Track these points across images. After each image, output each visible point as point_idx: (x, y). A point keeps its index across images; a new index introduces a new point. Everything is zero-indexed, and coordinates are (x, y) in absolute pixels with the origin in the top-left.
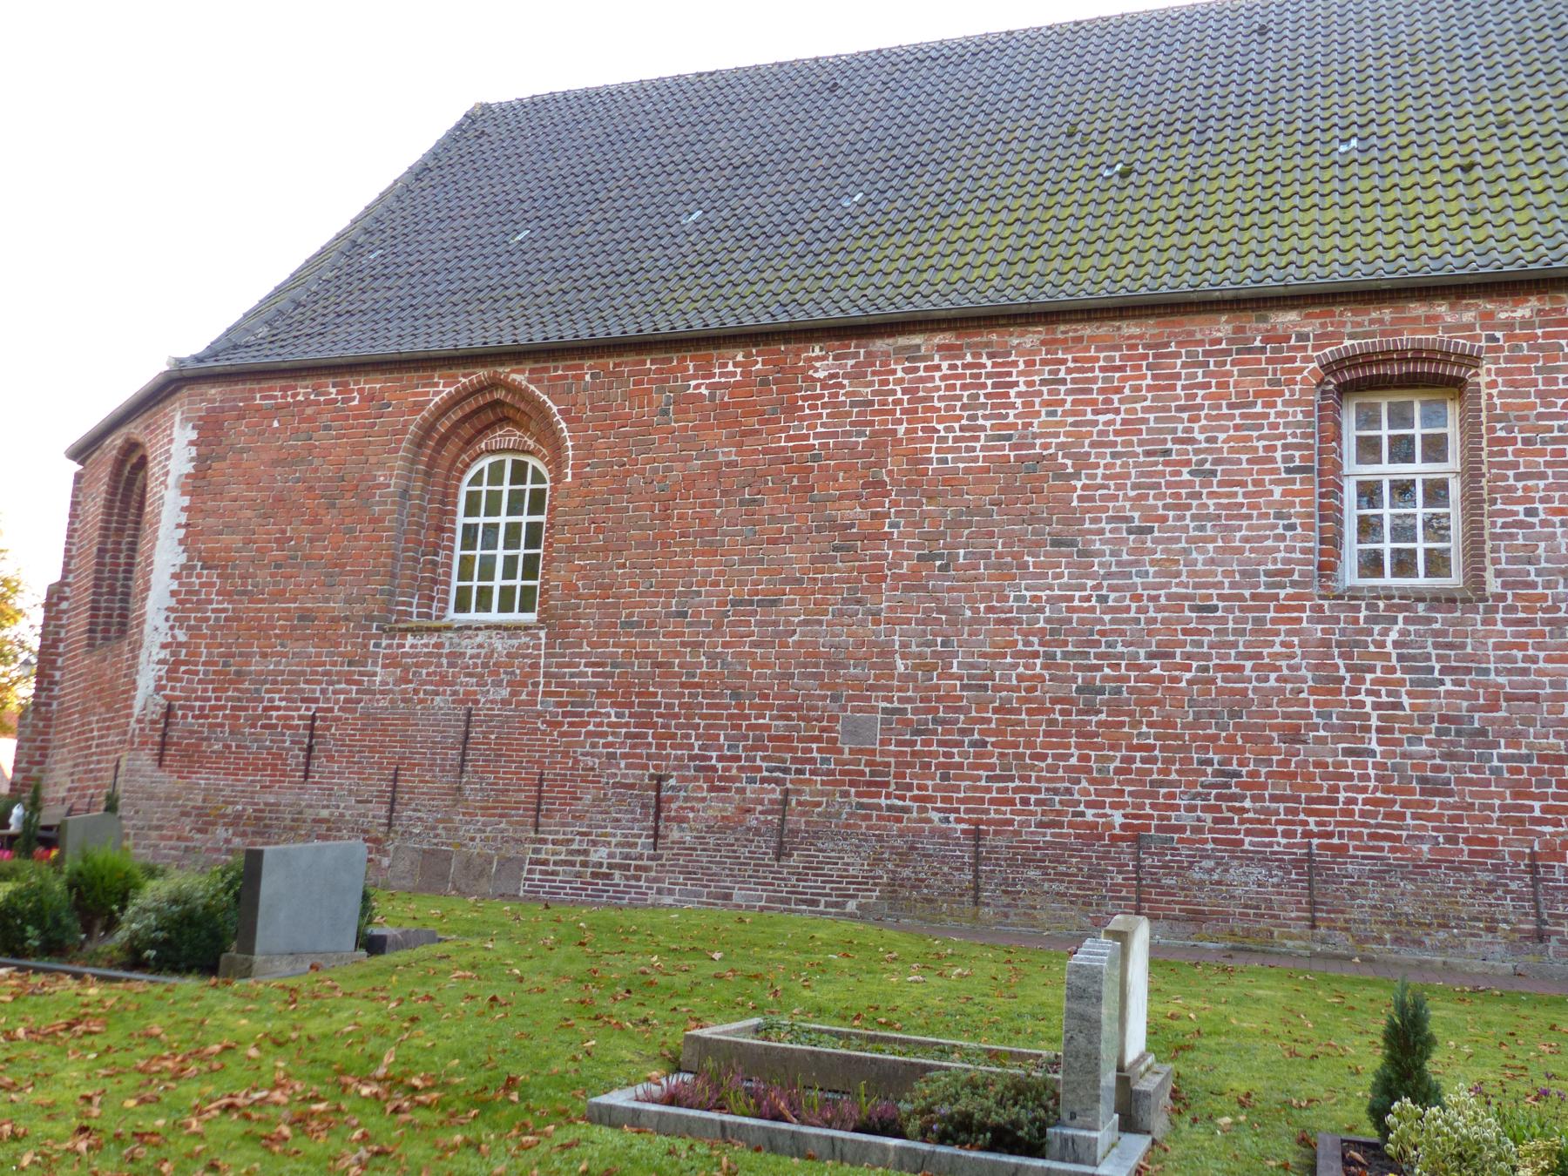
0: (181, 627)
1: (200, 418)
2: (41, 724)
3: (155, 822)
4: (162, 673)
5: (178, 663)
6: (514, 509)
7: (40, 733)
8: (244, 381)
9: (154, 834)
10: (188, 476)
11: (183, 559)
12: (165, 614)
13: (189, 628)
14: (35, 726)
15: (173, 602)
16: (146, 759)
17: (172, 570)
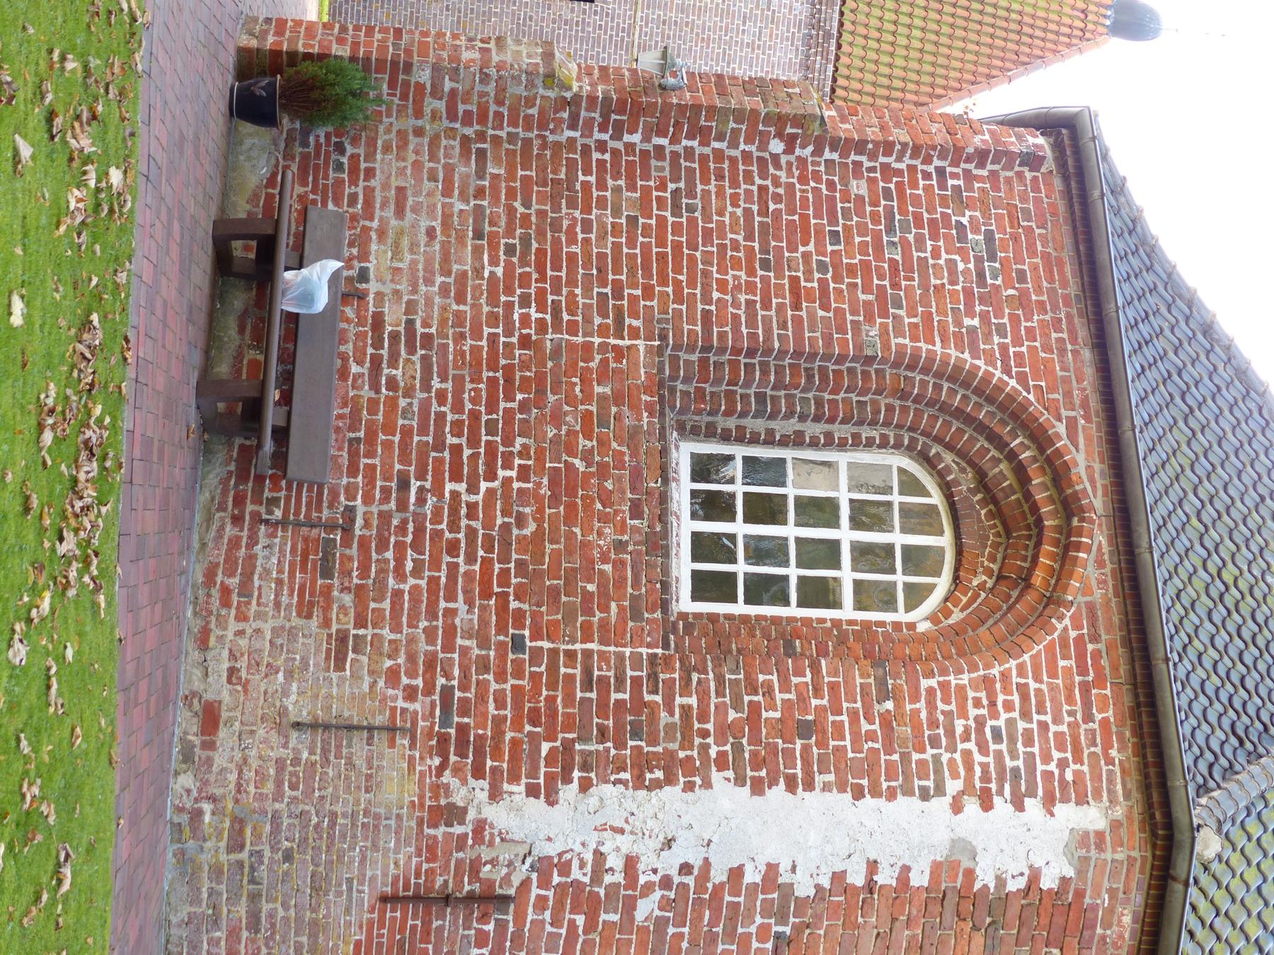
0: (665, 904)
1: (1080, 894)
2: (534, 111)
3: (266, 907)
4: (576, 874)
5: (592, 906)
6: (863, 554)
7: (514, 111)
8: (1115, 552)
9: (242, 910)
10: (970, 874)
11: (804, 889)
12: (697, 863)
13: (661, 923)
14: (530, 102)
15: (718, 875)
16: (395, 861)
17: (784, 866)
